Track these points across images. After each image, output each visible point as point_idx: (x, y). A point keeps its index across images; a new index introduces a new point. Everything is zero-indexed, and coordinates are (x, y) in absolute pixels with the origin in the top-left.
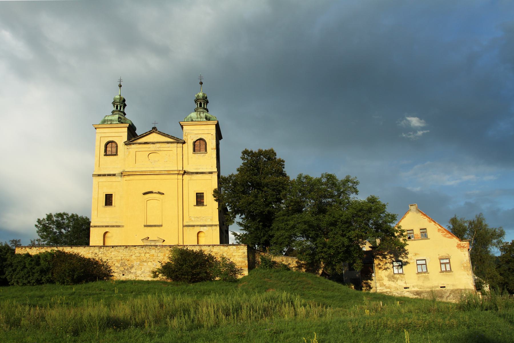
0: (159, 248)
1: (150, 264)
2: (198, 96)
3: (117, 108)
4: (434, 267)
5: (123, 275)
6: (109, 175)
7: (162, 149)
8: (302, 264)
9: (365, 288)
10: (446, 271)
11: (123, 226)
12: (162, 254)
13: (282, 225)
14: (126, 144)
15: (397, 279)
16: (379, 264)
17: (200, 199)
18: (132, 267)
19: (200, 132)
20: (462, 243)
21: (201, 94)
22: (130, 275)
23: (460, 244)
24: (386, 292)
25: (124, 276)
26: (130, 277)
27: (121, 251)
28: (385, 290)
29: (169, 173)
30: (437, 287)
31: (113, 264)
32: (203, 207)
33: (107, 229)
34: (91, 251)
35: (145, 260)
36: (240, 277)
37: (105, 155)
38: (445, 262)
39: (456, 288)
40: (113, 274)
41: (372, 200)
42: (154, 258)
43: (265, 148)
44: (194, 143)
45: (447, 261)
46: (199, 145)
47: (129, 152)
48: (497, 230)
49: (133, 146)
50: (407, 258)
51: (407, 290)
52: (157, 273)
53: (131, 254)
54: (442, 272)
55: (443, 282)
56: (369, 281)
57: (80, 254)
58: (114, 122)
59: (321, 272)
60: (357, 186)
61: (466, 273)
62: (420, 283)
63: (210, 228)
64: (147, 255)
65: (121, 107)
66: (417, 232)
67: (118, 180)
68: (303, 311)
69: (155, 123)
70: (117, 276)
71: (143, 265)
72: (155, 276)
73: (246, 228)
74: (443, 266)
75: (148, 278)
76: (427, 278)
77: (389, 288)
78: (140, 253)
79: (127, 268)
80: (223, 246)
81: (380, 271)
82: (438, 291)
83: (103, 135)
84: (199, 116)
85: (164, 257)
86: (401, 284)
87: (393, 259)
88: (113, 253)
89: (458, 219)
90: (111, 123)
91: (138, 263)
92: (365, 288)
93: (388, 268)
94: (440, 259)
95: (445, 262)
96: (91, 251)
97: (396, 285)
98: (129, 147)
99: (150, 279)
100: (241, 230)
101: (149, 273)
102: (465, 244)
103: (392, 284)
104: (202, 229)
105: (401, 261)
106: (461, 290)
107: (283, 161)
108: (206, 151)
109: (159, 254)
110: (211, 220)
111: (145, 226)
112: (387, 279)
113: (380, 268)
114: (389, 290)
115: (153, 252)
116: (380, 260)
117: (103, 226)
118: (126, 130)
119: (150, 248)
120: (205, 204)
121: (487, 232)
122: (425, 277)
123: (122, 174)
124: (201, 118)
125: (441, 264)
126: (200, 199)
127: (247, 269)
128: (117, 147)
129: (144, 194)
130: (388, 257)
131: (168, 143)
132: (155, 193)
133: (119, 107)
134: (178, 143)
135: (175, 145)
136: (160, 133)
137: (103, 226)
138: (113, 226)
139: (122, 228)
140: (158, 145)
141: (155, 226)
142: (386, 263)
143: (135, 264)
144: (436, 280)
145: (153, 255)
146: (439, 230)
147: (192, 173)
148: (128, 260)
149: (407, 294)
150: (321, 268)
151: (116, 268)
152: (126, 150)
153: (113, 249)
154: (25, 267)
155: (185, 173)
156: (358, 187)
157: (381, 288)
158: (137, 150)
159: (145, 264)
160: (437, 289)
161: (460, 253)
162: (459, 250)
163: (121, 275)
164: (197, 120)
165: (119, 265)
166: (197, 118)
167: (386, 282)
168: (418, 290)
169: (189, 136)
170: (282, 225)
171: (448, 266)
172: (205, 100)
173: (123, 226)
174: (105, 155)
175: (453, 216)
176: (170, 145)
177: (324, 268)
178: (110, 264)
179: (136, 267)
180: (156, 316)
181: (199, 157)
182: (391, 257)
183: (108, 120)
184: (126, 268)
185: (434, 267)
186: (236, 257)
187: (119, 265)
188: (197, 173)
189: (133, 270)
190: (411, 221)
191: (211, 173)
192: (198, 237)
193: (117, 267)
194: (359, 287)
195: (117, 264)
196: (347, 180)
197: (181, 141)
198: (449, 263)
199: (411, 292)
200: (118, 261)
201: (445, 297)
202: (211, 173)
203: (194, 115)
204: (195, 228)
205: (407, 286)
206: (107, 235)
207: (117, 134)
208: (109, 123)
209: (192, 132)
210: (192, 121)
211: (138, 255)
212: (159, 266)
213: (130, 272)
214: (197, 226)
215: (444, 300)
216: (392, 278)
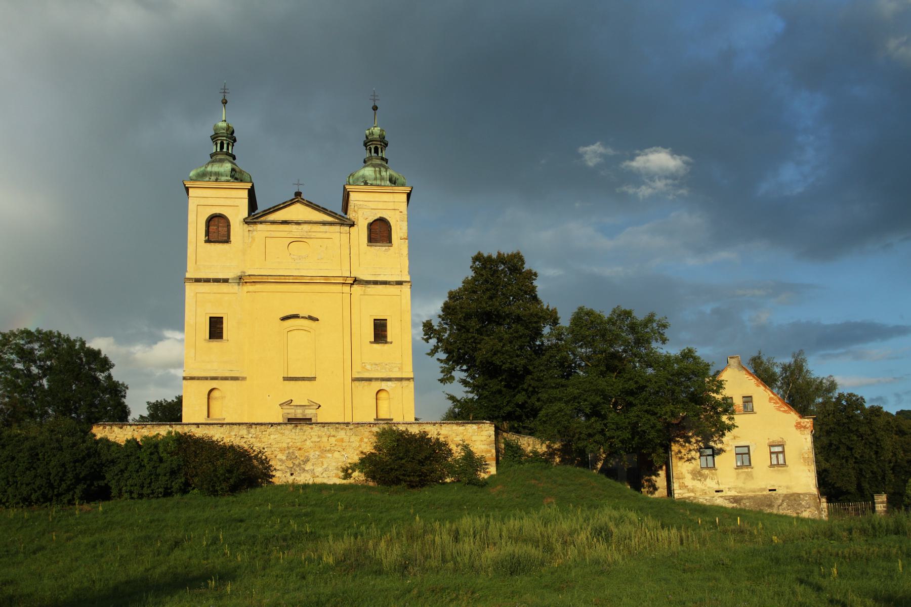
0: (352, 427)
1: (336, 454)
2: (372, 134)
3: (222, 147)
4: (760, 457)
5: (292, 474)
8: (556, 449)
9: (646, 490)
10: (778, 464)
11: (244, 379)
12: (358, 438)
13: (556, 393)
14: (246, 222)
15: (705, 477)
16: (680, 452)
17: (380, 331)
18: (307, 461)
19: (380, 206)
20: (803, 420)
21: (377, 130)
23: (799, 423)
24: (689, 498)
25: (293, 477)
26: (303, 478)
27: (287, 432)
28: (687, 495)
29: (327, 281)
30: (764, 490)
31: (273, 456)
32: (386, 346)
33: (214, 384)
34: (233, 434)
35: (328, 448)
36: (483, 476)
37: (206, 242)
38: (777, 450)
39: (790, 491)
40: (274, 473)
41: (688, 355)
42: (344, 444)
43: (507, 250)
45: (780, 449)
47: (253, 239)
48: (824, 381)
49: (259, 227)
50: (722, 442)
51: (720, 494)
52: (350, 471)
53: (305, 437)
54: (772, 466)
55: (772, 483)
56: (654, 477)
58: (224, 178)
59: (599, 465)
60: (666, 331)
61: (806, 468)
62: (740, 484)
63: (398, 383)
64: (332, 440)
65: (228, 144)
66: (738, 402)
68: (582, 529)
69: (298, 184)
70: (280, 477)
72: (347, 476)
73: (475, 388)
74: (774, 456)
75: (334, 478)
76: (750, 476)
77: (693, 491)
78: (319, 437)
79: (298, 462)
80: (457, 424)
81: (680, 463)
82: (765, 496)
83: (202, 202)
84: (378, 175)
85: (363, 444)
86: (711, 484)
87: (701, 444)
88: (272, 437)
89: (764, 359)
90: (216, 180)
91: (317, 453)
92: (646, 490)
93: (693, 458)
94: (771, 446)
95: (777, 450)
96: (233, 434)
97: (703, 487)
98: (252, 227)
99: (339, 481)
100: (467, 392)
102: (808, 422)
103: (698, 485)
104: (384, 385)
105: (712, 448)
109: (353, 439)
110: (401, 369)
111: (286, 379)
112: (690, 476)
113: (681, 458)
114: (692, 494)
115: (342, 434)
116: (681, 445)
117: (206, 378)
119: (337, 428)
120: (389, 340)
121: (809, 383)
122: (747, 474)
123: (241, 280)
124: (382, 179)
125: (771, 453)
127: (494, 463)
128: (229, 225)
129: (284, 319)
130: (693, 440)
131: (324, 223)
133: (225, 146)
134: (342, 224)
136: (310, 204)
137: (206, 378)
138: (226, 379)
139: (243, 382)
140: (306, 227)
141: (303, 379)
142: (690, 450)
143: (311, 456)
144: (762, 480)
145: (342, 440)
146: (771, 399)
147: (368, 282)
148: (300, 449)
149: (719, 501)
150: (600, 460)
151: (279, 463)
152: (247, 233)
153: (272, 429)
154: (142, 466)
155: (356, 281)
156: (667, 333)
157: (680, 491)
158: (268, 234)
159: (330, 455)
160: (765, 493)
161: (798, 437)
162: (798, 432)
163: (289, 474)
164: (374, 182)
165: (284, 458)
166: (376, 179)
167: (689, 481)
168: (737, 494)
169: (360, 212)
170: (556, 393)
171: (781, 456)
172: (383, 142)
173: (244, 379)
174: (206, 242)
175: (755, 354)
176: (327, 228)
177: (606, 461)
178: (268, 452)
179: (312, 461)
181: (379, 250)
182: (697, 442)
183: (211, 174)
184: (297, 463)
185: (760, 457)
186: (478, 443)
187: (284, 458)
188: (376, 283)
189: (308, 467)
190: (736, 383)
193: (281, 460)
194: (637, 487)
195: (280, 456)
196: (650, 319)
197: (349, 222)
198: (783, 452)
199: (724, 498)
200: (282, 450)
201: (776, 506)
202: (400, 283)
203: (369, 172)
204: (374, 383)
205: (721, 487)
206: (215, 394)
207: (228, 202)
208: (213, 178)
209: (368, 204)
210: (366, 184)
211: (315, 439)
212: (356, 459)
213: (304, 470)
214: (377, 379)
215: (775, 511)
216: (697, 475)
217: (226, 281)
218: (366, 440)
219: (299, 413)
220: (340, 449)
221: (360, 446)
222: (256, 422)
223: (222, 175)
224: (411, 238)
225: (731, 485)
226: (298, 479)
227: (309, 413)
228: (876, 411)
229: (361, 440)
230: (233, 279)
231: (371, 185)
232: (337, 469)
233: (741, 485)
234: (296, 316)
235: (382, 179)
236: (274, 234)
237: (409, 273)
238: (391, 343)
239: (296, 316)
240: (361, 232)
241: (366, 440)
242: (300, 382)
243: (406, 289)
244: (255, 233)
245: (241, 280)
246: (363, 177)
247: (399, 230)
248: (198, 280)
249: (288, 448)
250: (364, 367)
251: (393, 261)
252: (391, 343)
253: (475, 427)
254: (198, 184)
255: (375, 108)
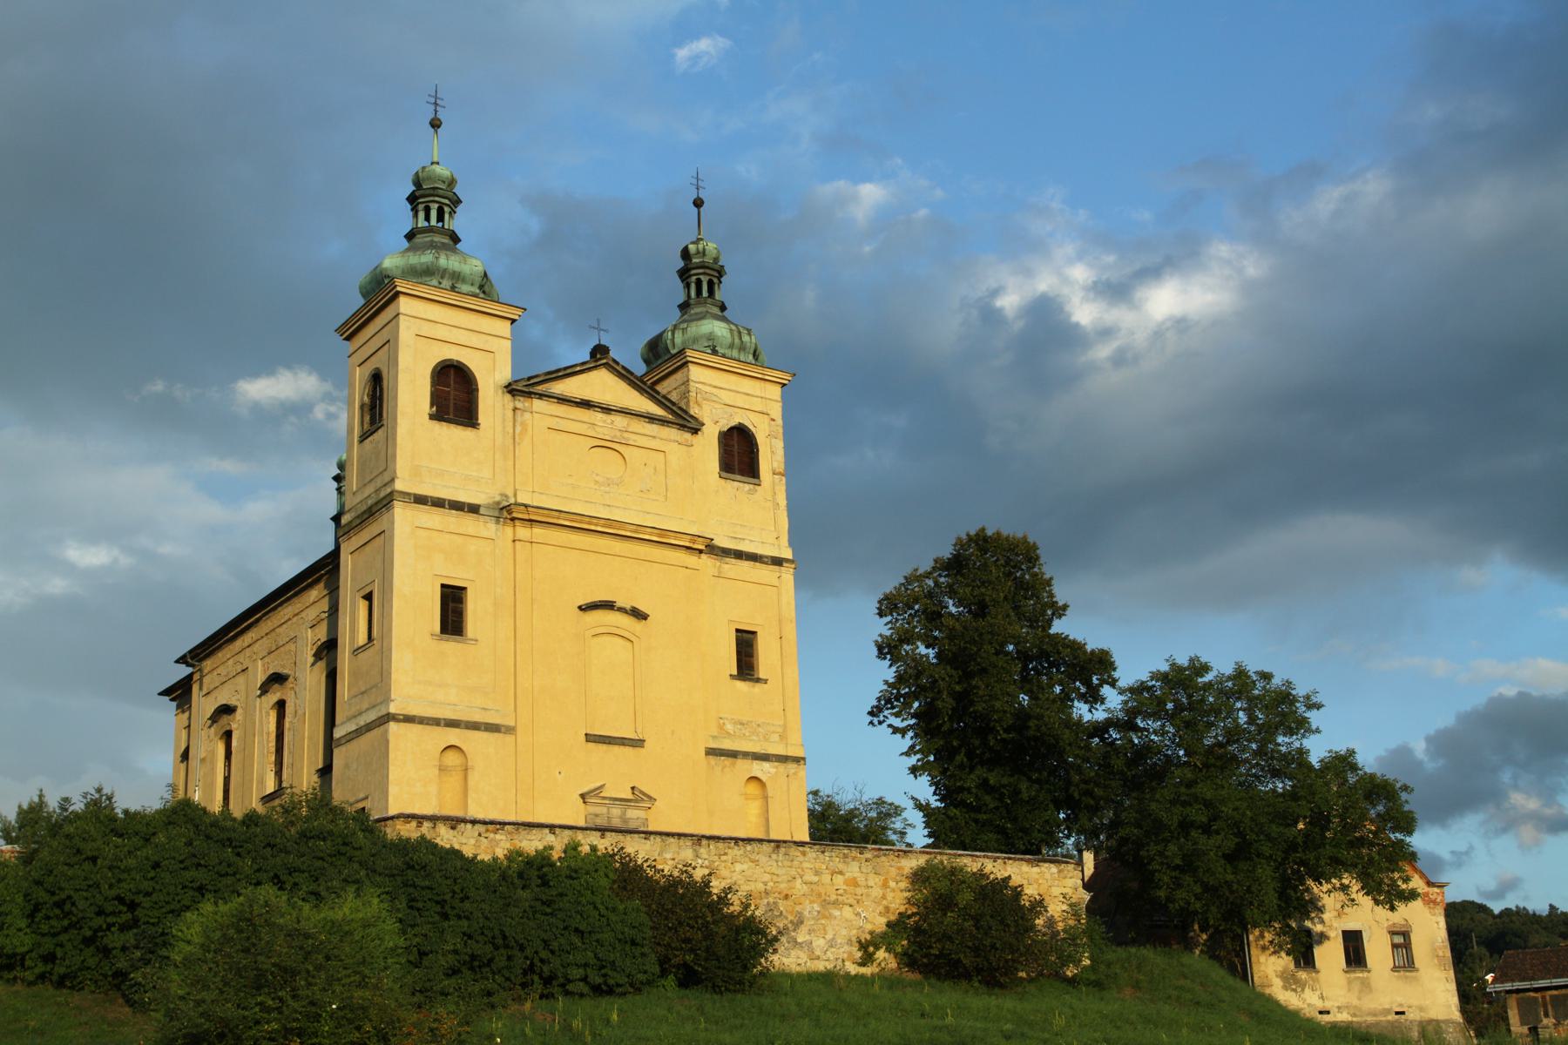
1: (847, 912)
7: (633, 439)
12: (878, 880)
18: (799, 923)
19: (740, 401)
22: (793, 953)
27: (763, 859)
30: (1388, 1011)
35: (833, 897)
42: (859, 891)
49: (538, 404)
50: (1322, 922)
53: (793, 872)
55: (1399, 999)
57: (53, 803)
61: (1443, 975)
63: (782, 768)
64: (839, 879)
67: (485, 534)
71: (830, 917)
72: (867, 959)
80: (1028, 861)
81: (1262, 959)
83: (427, 329)
84: (737, 341)
88: (738, 867)
90: (453, 288)
98: (521, 403)
99: (853, 969)
101: (846, 948)
106: (1438, 1021)
107: (432, 417)
110: (783, 737)
111: (590, 738)
113: (1264, 948)
117: (436, 722)
124: (742, 348)
131: (651, 419)
132: (621, 610)
137: (436, 722)
140: (620, 421)
143: (806, 913)
145: (854, 883)
147: (726, 553)
148: (786, 897)
150: (1197, 945)
153: (736, 852)
158: (554, 423)
159: (837, 913)
164: (728, 352)
166: (731, 346)
169: (706, 407)
176: (654, 429)
179: (809, 923)
181: (736, 488)
183: (443, 273)
188: (739, 555)
202: (778, 562)
205: (1328, 1005)
207: (475, 340)
210: (714, 352)
212: (880, 924)
214: (746, 755)
217: (474, 509)
218: (892, 884)
219: (615, 815)
220: (851, 901)
221: (884, 897)
222: (708, 833)
223: (464, 281)
224: (792, 471)
225: (1342, 1001)
226: (785, 960)
227: (635, 815)
228: (473, 861)
229: (885, 885)
230: (488, 507)
231: (724, 356)
232: (850, 942)
233: (1355, 1002)
234: (608, 606)
235: (742, 348)
236: (564, 425)
237: (791, 544)
238: (765, 681)
239: (608, 606)
240: (707, 448)
241: (892, 884)
242: (616, 749)
243: (787, 574)
244: (527, 416)
245: (507, 512)
246: (710, 337)
247: (771, 455)
248: (420, 500)
249: (767, 893)
250: (721, 727)
251: (758, 515)
252: (765, 681)
253: (1054, 869)
254: (421, 290)
255: (435, 124)
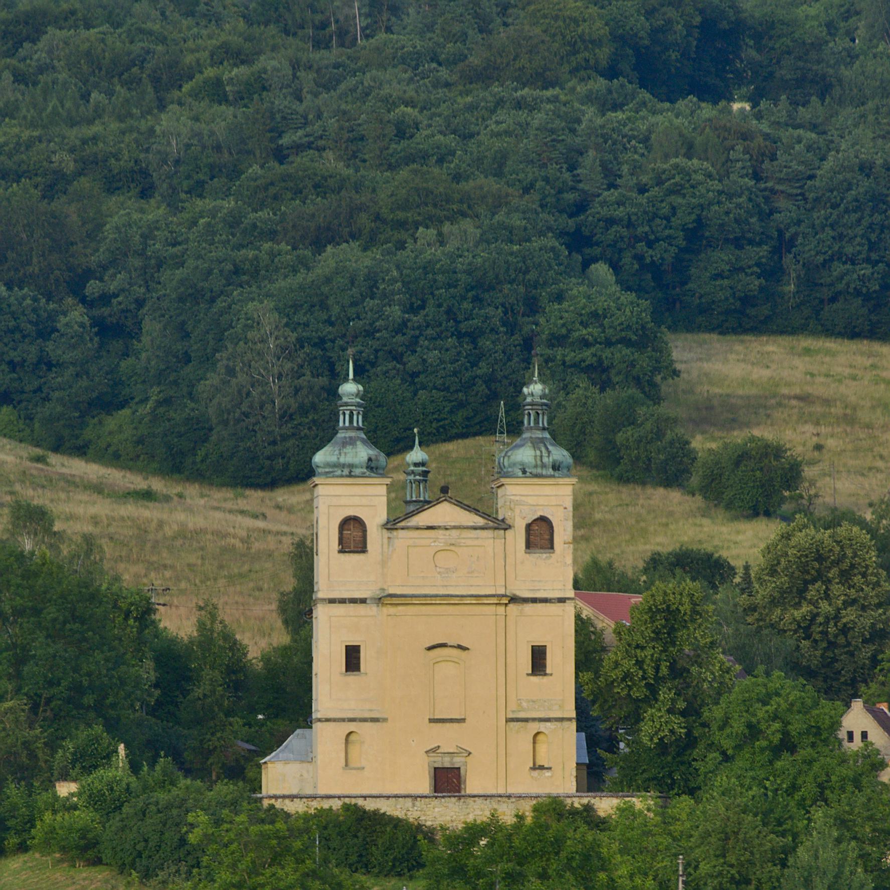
6: (353, 601)
11: (385, 720)
17: (539, 659)
32: (545, 679)
33: (352, 727)
44: (529, 527)
46: (540, 534)
49: (401, 533)
63: (558, 724)
104: (542, 727)
108: (552, 548)
110: (561, 707)
111: (432, 721)
117: (343, 720)
118: (383, 490)
120: (548, 671)
126: (539, 659)
135: (488, 533)
137: (343, 720)
138: (364, 720)
139: (384, 724)
141: (451, 721)
147: (525, 600)
158: (411, 542)
173: (385, 720)
174: (340, 552)
180: (269, 660)
181: (539, 560)
188: (534, 600)
191: (562, 600)
192: (534, 742)
202: (562, 600)
207: (364, 501)
208: (346, 472)
214: (534, 720)
